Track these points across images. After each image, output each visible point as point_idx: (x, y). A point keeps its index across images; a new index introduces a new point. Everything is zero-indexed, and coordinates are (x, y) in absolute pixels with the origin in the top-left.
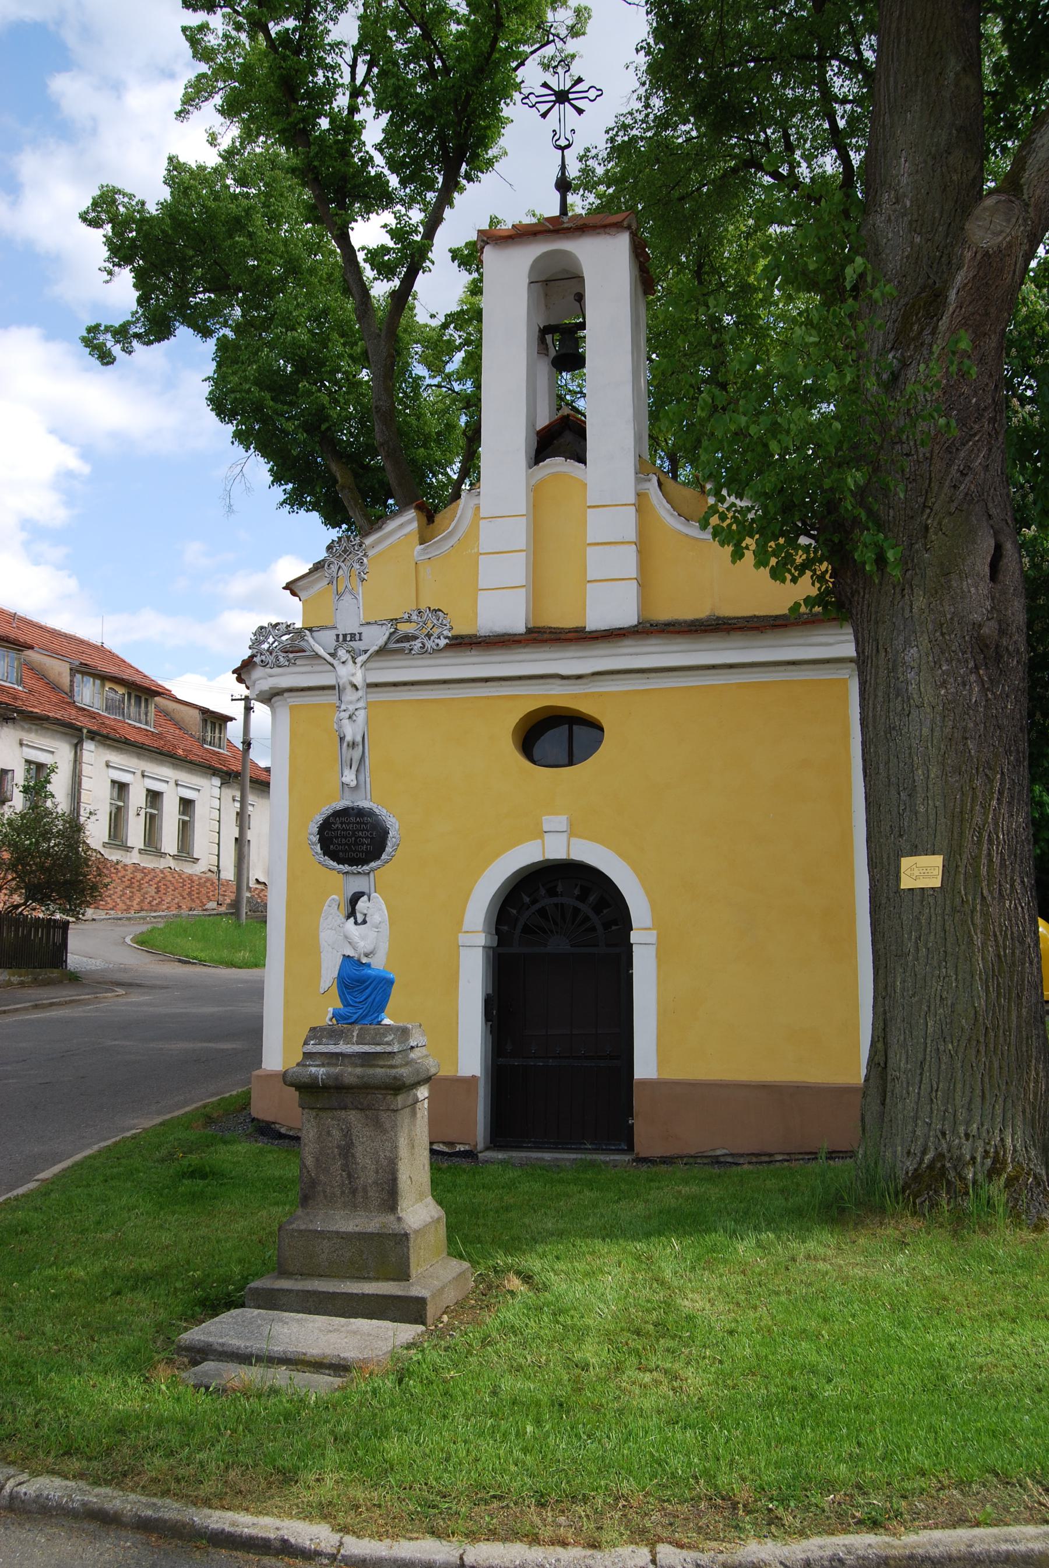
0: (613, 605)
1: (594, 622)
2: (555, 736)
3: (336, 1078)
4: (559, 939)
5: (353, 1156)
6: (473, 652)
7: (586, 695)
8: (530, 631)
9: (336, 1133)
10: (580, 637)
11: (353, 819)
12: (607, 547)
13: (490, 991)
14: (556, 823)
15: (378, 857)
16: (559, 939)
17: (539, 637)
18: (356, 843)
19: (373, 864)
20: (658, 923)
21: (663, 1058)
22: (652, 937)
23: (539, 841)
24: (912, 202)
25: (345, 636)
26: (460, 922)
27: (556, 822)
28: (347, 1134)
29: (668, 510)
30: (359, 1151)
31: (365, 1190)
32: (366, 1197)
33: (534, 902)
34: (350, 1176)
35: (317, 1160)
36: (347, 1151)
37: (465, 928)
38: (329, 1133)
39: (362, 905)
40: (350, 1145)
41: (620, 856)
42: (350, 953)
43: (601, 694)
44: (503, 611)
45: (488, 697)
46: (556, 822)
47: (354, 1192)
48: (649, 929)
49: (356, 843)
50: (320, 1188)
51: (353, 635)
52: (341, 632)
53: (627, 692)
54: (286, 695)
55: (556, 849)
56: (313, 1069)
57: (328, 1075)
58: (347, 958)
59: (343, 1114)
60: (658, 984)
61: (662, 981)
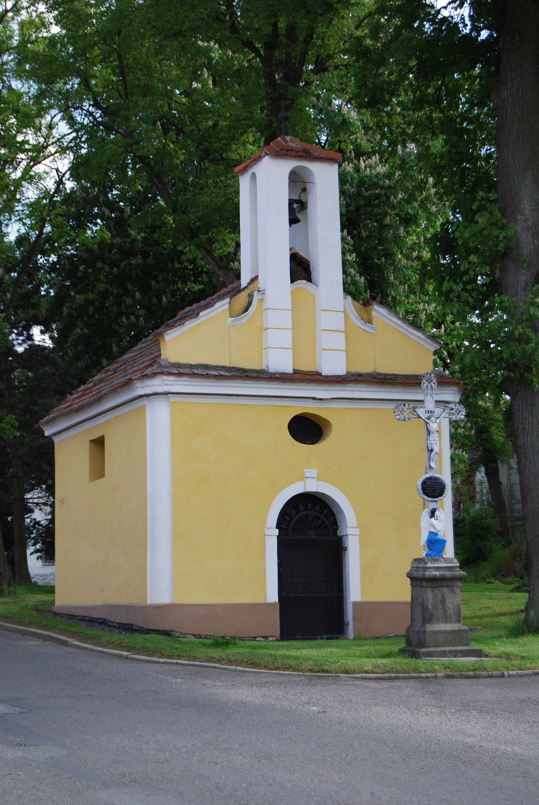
0: (334, 364)
1: (327, 370)
2: (307, 429)
3: (443, 575)
4: (310, 532)
5: (445, 604)
6: (276, 383)
7: (324, 408)
8: (296, 372)
9: (439, 596)
10: (315, 378)
11: (433, 481)
12: (332, 332)
13: (345, 553)
14: (309, 473)
15: (442, 495)
16: (310, 532)
17: (299, 377)
18: (435, 490)
19: (440, 498)
20: (359, 525)
21: (363, 592)
22: (357, 531)
23: (302, 482)
24: (532, 224)
25: (428, 411)
26: (265, 523)
27: (312, 472)
28: (443, 596)
29: (355, 316)
30: (447, 602)
31: (450, 616)
32: (450, 618)
33: (297, 513)
34: (445, 611)
35: (433, 606)
36: (443, 602)
37: (267, 526)
38: (437, 596)
39: (437, 513)
40: (444, 600)
41: (341, 491)
42: (433, 530)
43: (331, 409)
44: (281, 361)
45: (275, 406)
46: (312, 472)
47: (446, 617)
48: (355, 528)
49: (435, 490)
50: (434, 616)
51: (431, 411)
52: (427, 410)
53: (343, 409)
54: (169, 395)
55: (312, 486)
56: (434, 573)
57: (440, 574)
58: (431, 533)
59: (441, 589)
60: (360, 555)
61: (362, 553)
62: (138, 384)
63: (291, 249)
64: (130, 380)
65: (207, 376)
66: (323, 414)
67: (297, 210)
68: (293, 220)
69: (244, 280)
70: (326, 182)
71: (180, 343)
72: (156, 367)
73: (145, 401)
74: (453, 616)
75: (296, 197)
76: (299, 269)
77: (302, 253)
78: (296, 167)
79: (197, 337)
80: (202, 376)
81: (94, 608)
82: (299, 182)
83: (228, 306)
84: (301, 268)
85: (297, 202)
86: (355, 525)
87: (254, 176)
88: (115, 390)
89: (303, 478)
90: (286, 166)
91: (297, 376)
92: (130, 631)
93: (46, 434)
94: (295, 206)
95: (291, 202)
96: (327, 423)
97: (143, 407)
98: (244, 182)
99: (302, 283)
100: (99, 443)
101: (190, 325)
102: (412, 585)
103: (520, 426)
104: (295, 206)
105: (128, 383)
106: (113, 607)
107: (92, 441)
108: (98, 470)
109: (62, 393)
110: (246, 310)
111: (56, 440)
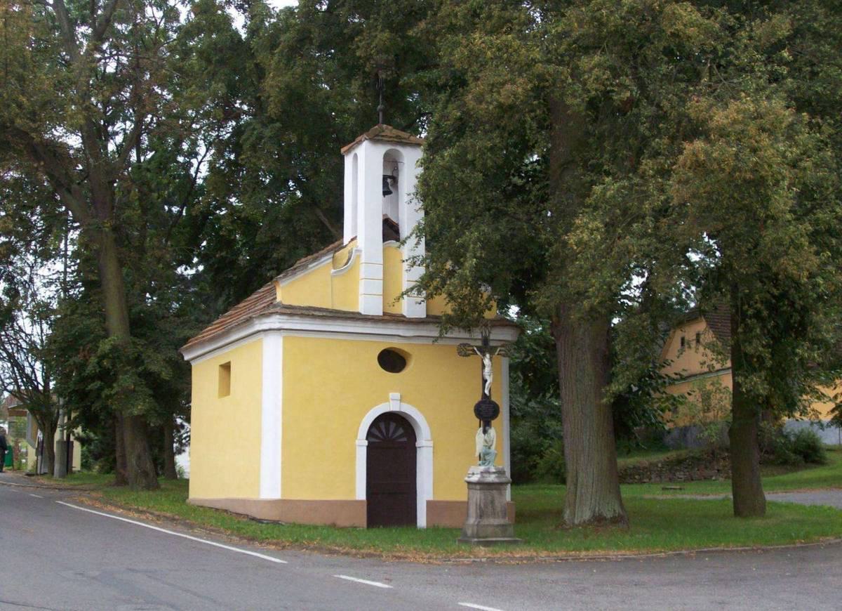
2: (392, 361)
4: (392, 443)
28: (493, 497)
36: (492, 502)
62: (257, 322)
63: (384, 215)
64: (250, 317)
65: (314, 317)
66: (406, 349)
67: (390, 184)
68: (386, 192)
69: (346, 239)
70: (411, 163)
71: (288, 290)
72: (272, 308)
73: (262, 336)
74: (500, 514)
75: (389, 174)
76: (391, 231)
77: (394, 220)
78: (390, 150)
79: (300, 287)
80: (308, 316)
81: (219, 501)
82: (392, 162)
83: (331, 260)
84: (391, 230)
85: (390, 177)
86: (429, 438)
87: (356, 156)
88: (240, 326)
89: (387, 400)
90: (381, 150)
91: (386, 318)
92: (618, 493)
93: (186, 358)
94: (389, 180)
95: (385, 178)
96: (409, 355)
97: (260, 341)
98: (348, 161)
99: (393, 243)
100: (226, 367)
101: (300, 275)
102: (468, 488)
103: (562, 362)
104: (389, 180)
105: (249, 321)
106: (233, 501)
107: (221, 366)
108: (225, 388)
109: (201, 324)
110: (346, 264)
111: (193, 364)
